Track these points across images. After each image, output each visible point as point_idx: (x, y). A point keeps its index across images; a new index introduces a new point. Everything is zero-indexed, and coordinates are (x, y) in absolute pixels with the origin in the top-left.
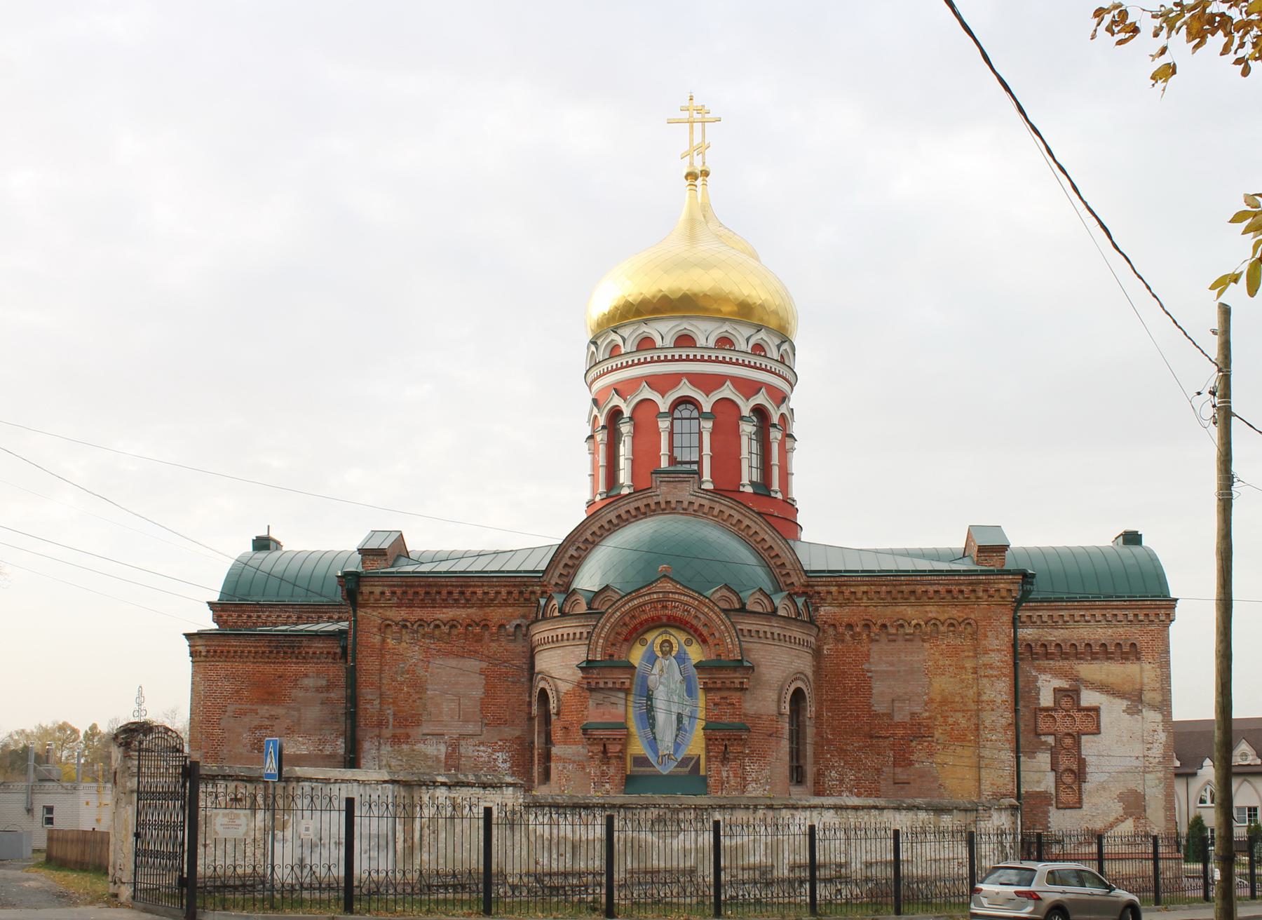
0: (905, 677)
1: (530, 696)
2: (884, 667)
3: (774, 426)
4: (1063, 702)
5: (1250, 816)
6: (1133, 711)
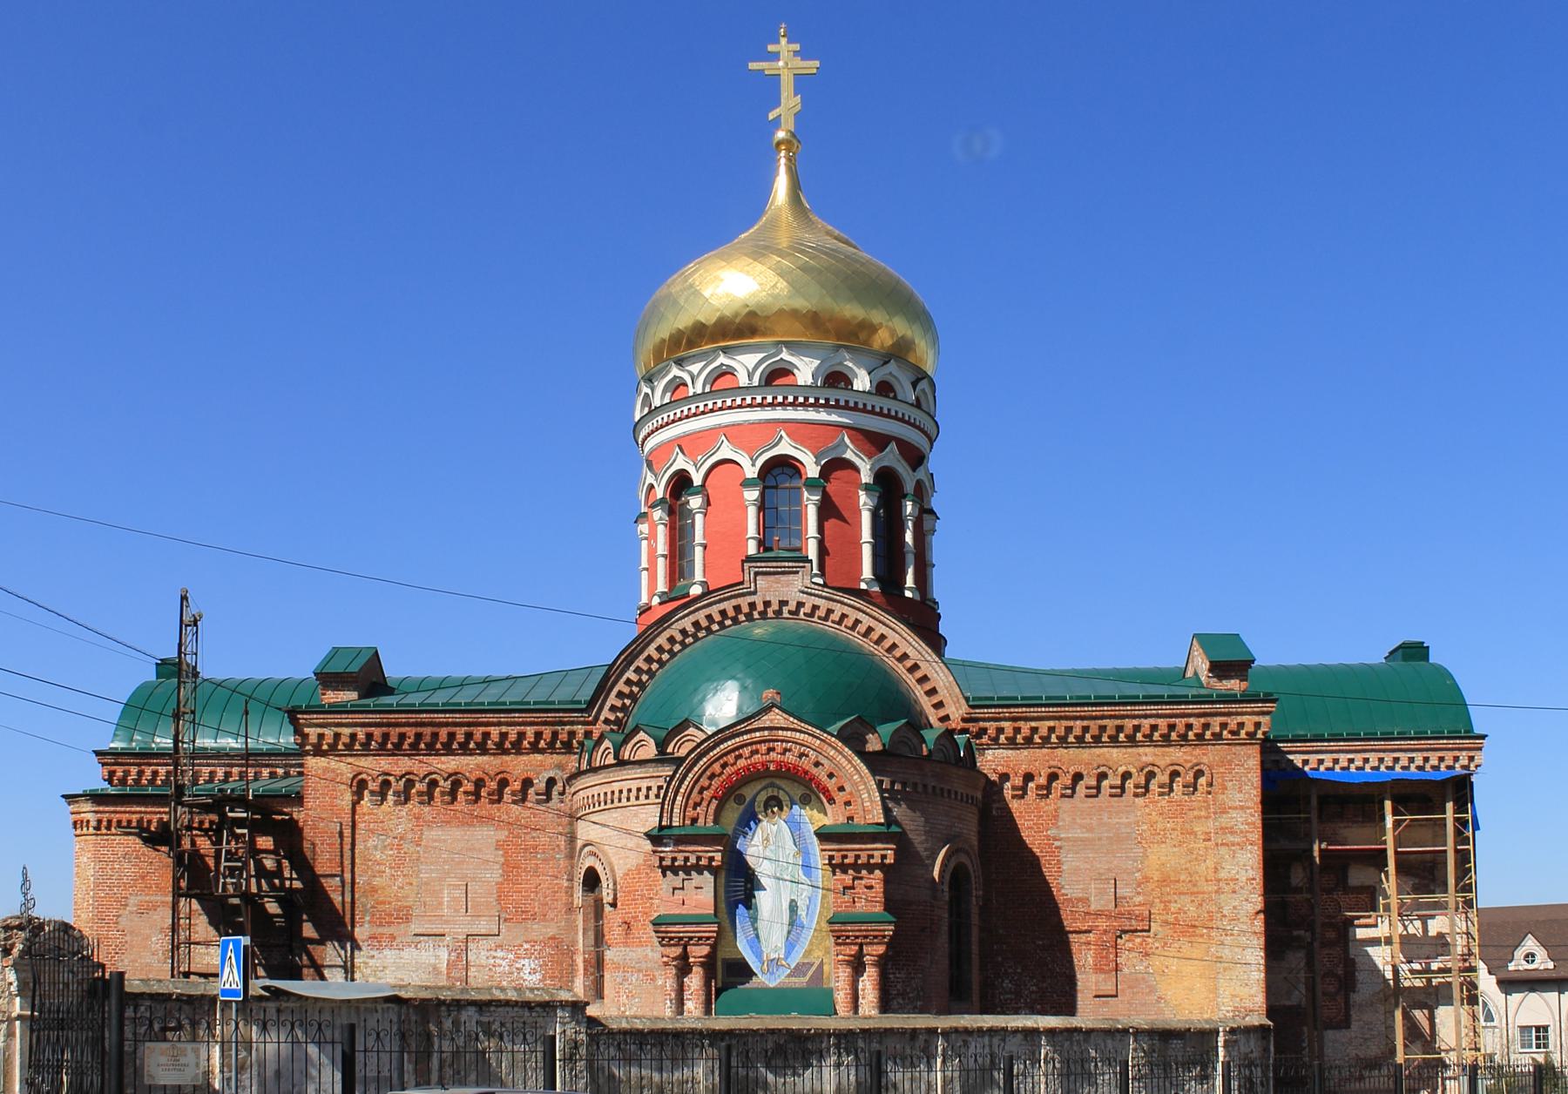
1: (571, 880)
2: (1078, 833)
5: (1538, 1038)
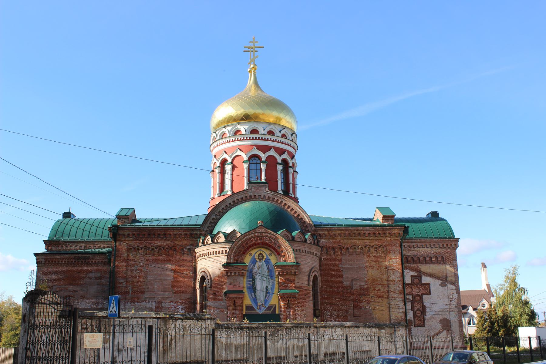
0: (358, 270)
2: (347, 266)
3: (290, 167)
4: (415, 281)
6: (443, 285)
